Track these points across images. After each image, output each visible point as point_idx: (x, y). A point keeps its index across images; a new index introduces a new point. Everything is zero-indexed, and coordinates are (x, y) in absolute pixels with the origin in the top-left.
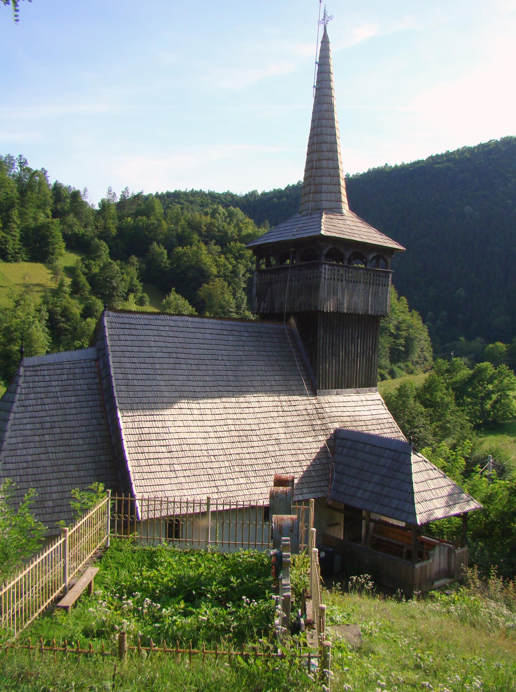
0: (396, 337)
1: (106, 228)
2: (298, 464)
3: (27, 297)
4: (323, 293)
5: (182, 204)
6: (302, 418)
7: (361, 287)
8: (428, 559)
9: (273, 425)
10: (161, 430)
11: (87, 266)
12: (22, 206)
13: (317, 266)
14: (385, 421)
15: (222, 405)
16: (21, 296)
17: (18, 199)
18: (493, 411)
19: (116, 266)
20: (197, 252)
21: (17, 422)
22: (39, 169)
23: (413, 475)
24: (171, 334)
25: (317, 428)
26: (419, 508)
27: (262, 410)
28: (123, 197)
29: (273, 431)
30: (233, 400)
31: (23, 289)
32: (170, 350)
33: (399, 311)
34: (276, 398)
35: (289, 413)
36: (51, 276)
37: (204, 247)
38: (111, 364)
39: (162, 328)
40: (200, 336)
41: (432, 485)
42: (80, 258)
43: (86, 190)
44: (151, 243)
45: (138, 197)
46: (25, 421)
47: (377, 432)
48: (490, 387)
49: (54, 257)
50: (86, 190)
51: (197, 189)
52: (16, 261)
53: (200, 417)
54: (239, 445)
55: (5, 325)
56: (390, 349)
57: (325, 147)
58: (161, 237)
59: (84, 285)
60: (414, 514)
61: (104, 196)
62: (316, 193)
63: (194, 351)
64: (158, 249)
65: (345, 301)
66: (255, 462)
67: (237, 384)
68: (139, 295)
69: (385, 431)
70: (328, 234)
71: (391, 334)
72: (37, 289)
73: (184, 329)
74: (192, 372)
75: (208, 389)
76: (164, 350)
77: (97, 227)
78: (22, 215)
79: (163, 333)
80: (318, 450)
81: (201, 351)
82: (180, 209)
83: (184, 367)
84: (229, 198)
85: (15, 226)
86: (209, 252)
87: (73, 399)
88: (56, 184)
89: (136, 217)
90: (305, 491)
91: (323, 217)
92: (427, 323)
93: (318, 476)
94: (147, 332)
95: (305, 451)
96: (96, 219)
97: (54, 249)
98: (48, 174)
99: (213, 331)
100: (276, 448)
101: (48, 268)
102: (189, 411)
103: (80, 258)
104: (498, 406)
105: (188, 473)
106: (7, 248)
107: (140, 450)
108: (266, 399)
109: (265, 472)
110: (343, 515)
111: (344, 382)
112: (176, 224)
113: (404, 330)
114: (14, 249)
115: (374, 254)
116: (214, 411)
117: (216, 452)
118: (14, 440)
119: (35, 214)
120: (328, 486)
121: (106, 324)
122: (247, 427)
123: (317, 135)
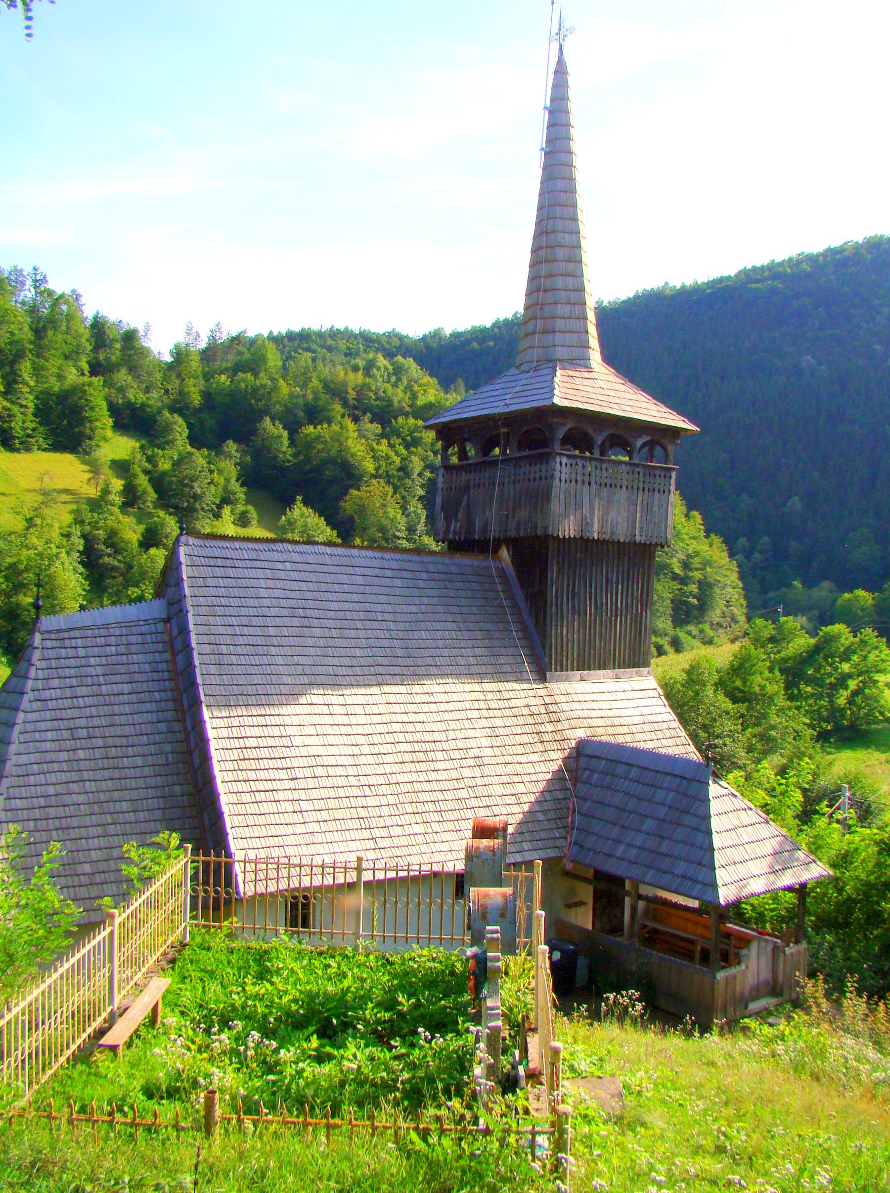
0: (683, 581)
2: (513, 800)
3: (46, 511)
4: (557, 505)
5: (314, 352)
6: (521, 720)
8: (739, 963)
9: (471, 733)
10: (278, 742)
11: (149, 459)
12: (38, 355)
13: (547, 458)
14: (664, 726)
16: (36, 510)
17: (31, 343)
18: (850, 709)
19: (200, 458)
20: (340, 434)
21: (30, 727)
23: (712, 820)
24: (295, 575)
25: (546, 737)
30: (402, 689)
31: (41, 498)
32: (293, 603)
34: (477, 687)
35: (498, 713)
36: (88, 476)
37: (351, 426)
38: (191, 627)
39: (279, 566)
40: (344, 579)
41: (745, 835)
43: (148, 328)
44: (261, 419)
45: (236, 340)
46: (43, 726)
47: (650, 745)
48: (846, 667)
49: (93, 443)
51: (340, 325)
52: (28, 450)
53: (346, 720)
56: (672, 602)
57: (561, 253)
58: (278, 408)
59: (144, 492)
60: (714, 886)
61: (180, 338)
62: (545, 332)
64: (273, 429)
65: (596, 520)
67: (410, 661)
68: (241, 508)
71: (675, 577)
72: (64, 497)
74: (331, 642)
76: (283, 603)
78: (37, 371)
81: (346, 606)
82: (310, 361)
83: (317, 632)
84: (396, 342)
85: (26, 389)
86: (361, 435)
87: (126, 688)
88: (96, 318)
89: (235, 374)
90: (526, 846)
92: (737, 557)
93: (549, 820)
95: (526, 778)
98: (83, 300)
99: (367, 571)
100: (477, 772)
102: (325, 709)
103: (138, 445)
104: (858, 700)
105: (324, 815)
106: (11, 428)
108: (460, 687)
110: (591, 888)
111: (589, 660)
112: (304, 386)
113: (697, 569)
114: (24, 429)
115: (646, 438)
116: (368, 709)
117: (373, 780)
118: (24, 759)
119: (60, 368)
120: (566, 838)
121: (183, 558)
122: (427, 737)
123: (546, 233)
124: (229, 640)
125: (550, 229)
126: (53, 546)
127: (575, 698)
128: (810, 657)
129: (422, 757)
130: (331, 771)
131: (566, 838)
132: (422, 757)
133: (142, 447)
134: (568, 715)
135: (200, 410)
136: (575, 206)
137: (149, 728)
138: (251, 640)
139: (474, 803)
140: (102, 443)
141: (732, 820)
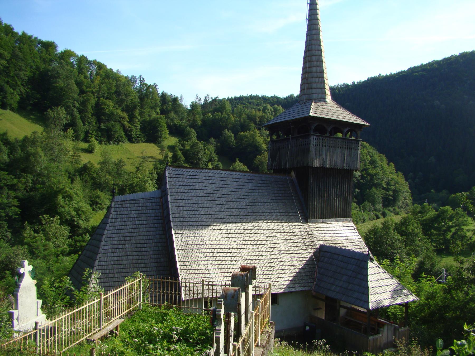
0: (387, 190)
1: (195, 121)
2: (292, 267)
3: (144, 165)
4: (312, 154)
5: (244, 104)
6: (297, 237)
7: (339, 150)
8: (379, 333)
9: (277, 242)
10: (200, 243)
11: (182, 145)
12: (142, 107)
13: (307, 136)
14: (356, 240)
15: (242, 228)
16: (140, 164)
17: (139, 103)
18: (452, 240)
19: (201, 145)
20: (253, 135)
21: (109, 236)
22: (152, 84)
23: (369, 276)
24: (210, 181)
25: (307, 244)
26: (372, 299)
27: (270, 231)
28: (206, 100)
29: (277, 245)
30: (250, 224)
31: (142, 160)
32: (209, 192)
33: (387, 172)
34: (280, 224)
35: (288, 234)
36: (159, 151)
37: (257, 132)
38: (169, 200)
39: (204, 178)
40: (229, 183)
41: (382, 283)
42: (178, 140)
43: (182, 97)
44: (223, 130)
45: (215, 100)
46: (114, 235)
47: (350, 248)
48: (450, 223)
49: (162, 139)
50: (182, 97)
51: (254, 94)
52: (138, 142)
53: (227, 235)
54: (253, 254)
55: (130, 182)
56: (382, 198)
57: (314, 58)
58: (230, 125)
59: (180, 157)
60: (368, 302)
61: (194, 100)
62: (308, 89)
63: (225, 193)
64: (228, 133)
65: (328, 160)
66: (263, 265)
67: (253, 214)
68: (216, 163)
69: (356, 247)
70: (315, 115)
71: (384, 188)
72: (150, 159)
73: (219, 179)
74: (223, 206)
75: (233, 217)
76: (205, 191)
77: (189, 120)
78: (141, 113)
79: (205, 181)
80: (308, 259)
81: (229, 193)
82: (242, 107)
83: (218, 202)
84: (275, 100)
85: (137, 120)
86: (261, 135)
87: (145, 222)
88: (162, 93)
89: (214, 113)
90: (297, 285)
91: (313, 104)
92: (409, 181)
93: (306, 276)
94: (194, 180)
95: (298, 259)
96: (188, 115)
97: (161, 135)
98: (158, 87)
99: (238, 180)
100: (278, 256)
101: (158, 147)
102: (219, 231)
103: (178, 140)
104: (456, 236)
105: (217, 271)
106: (132, 134)
107: (185, 255)
108: (273, 224)
109: (270, 272)
110: (324, 303)
111: (326, 215)
112: (240, 117)
113: (392, 185)
114: (136, 135)
115: (348, 129)
116: (236, 232)
117: (237, 258)
118: (106, 247)
119: (149, 112)
120: (313, 283)
121: (167, 175)
122: (259, 243)
123: (309, 51)
124: (183, 205)
125: (310, 49)
126: (146, 177)
127: (320, 229)
128: (435, 219)
129: (257, 250)
130: (221, 254)
131: (313, 283)
132: (257, 250)
133: (179, 141)
134: (316, 235)
135: (200, 127)
136: (320, 40)
137: (152, 237)
138: (192, 205)
139: (277, 268)
140: (165, 139)
141: (377, 277)
